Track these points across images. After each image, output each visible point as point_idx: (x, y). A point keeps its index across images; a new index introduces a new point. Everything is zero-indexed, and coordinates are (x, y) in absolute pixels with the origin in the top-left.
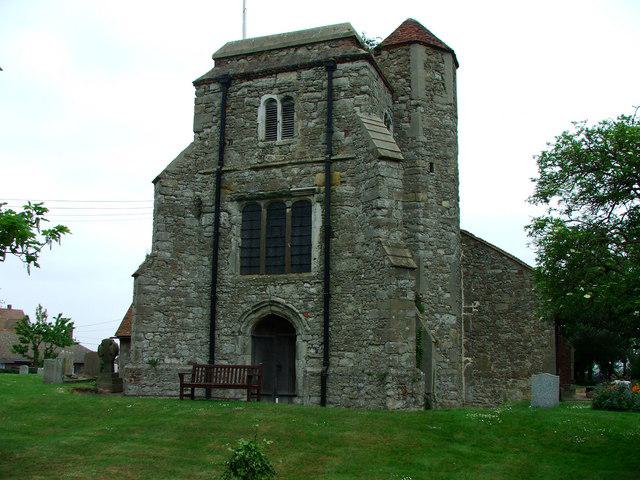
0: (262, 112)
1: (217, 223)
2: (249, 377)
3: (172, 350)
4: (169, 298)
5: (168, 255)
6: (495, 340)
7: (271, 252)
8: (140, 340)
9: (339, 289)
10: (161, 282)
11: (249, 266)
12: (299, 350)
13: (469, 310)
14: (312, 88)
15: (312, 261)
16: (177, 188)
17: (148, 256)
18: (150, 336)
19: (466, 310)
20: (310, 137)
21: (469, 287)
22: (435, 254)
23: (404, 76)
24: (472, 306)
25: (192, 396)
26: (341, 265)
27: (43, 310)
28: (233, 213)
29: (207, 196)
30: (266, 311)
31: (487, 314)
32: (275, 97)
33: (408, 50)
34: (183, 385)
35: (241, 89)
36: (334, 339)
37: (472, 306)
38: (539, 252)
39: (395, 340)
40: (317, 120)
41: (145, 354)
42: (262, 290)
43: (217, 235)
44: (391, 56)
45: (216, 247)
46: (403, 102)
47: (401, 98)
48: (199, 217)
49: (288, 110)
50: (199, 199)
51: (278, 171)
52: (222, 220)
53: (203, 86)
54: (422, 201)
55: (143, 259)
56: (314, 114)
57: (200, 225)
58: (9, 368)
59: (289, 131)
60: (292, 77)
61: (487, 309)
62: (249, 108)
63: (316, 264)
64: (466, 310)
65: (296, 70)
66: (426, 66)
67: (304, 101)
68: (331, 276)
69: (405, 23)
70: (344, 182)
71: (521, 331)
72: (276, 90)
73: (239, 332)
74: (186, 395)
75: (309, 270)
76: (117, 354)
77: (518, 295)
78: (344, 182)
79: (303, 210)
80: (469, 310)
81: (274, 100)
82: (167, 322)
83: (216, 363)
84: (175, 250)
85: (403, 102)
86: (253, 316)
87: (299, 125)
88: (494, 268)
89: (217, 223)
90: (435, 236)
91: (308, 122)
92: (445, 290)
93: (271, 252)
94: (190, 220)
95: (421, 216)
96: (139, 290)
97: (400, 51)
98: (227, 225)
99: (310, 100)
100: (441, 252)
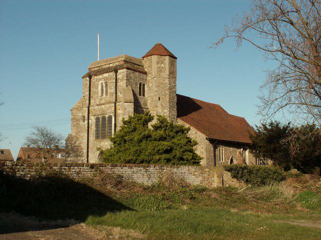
0: (100, 87)
11: (97, 137)
28: (93, 120)
35: (94, 78)
43: (88, 127)
51: (104, 106)
56: (113, 87)
59: (106, 94)
60: (106, 75)
66: (158, 63)
79: (110, 117)
87: (109, 91)
94: (81, 123)
97: (149, 58)
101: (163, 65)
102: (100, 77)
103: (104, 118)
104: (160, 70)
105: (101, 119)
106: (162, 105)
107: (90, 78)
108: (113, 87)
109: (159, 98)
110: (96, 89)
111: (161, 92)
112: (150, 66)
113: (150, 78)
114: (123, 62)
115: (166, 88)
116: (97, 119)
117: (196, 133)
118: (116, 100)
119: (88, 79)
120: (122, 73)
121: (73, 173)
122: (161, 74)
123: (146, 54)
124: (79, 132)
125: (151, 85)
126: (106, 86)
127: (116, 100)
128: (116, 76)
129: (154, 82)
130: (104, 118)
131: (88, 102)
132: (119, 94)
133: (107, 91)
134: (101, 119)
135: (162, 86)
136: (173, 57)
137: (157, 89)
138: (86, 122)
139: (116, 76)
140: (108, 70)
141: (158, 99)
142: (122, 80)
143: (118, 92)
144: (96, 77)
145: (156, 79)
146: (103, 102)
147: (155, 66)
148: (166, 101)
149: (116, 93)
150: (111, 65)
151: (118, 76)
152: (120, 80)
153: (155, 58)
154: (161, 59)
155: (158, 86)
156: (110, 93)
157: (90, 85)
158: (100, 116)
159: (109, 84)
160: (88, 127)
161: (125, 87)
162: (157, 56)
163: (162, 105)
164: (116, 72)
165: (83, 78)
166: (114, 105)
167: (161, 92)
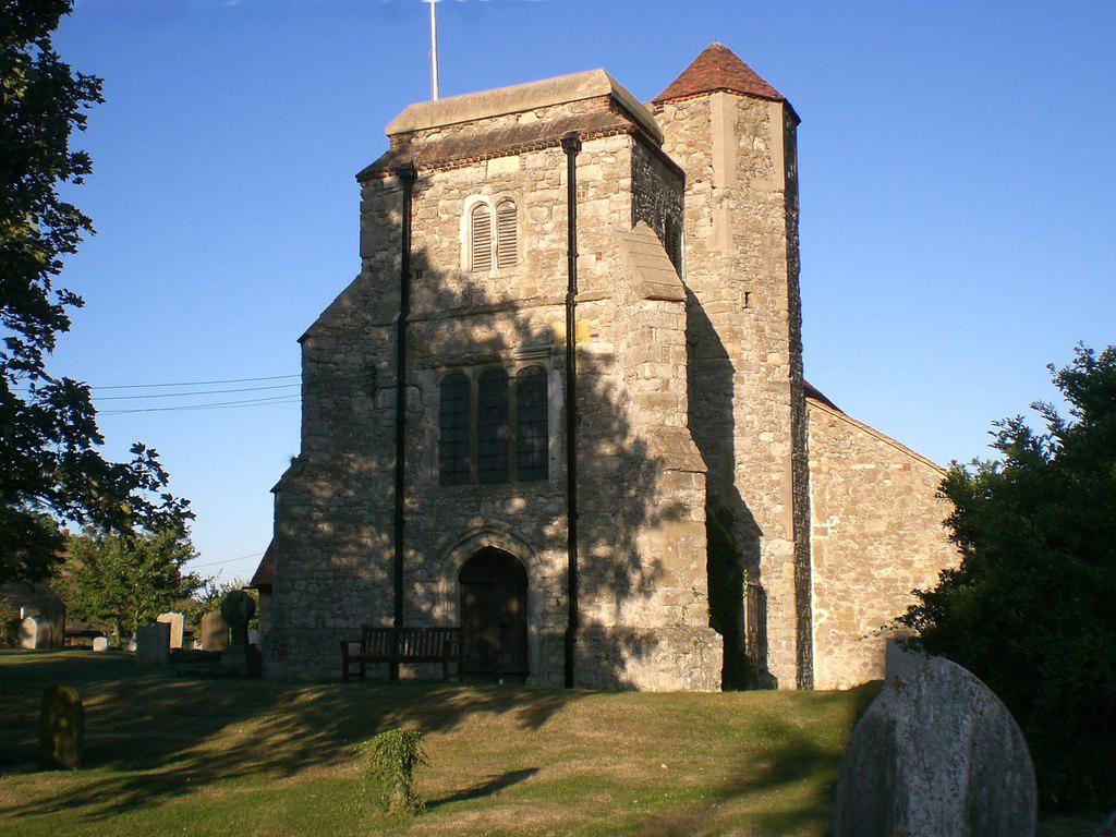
0: (465, 224)
1: (401, 405)
3: (336, 606)
5: (327, 457)
6: (866, 578)
9: (591, 505)
13: (824, 532)
14: (544, 184)
15: (550, 462)
17: (294, 460)
21: (822, 492)
24: (828, 525)
25: (362, 676)
27: (69, 310)
28: (426, 389)
31: (853, 537)
32: (485, 199)
33: (706, 103)
34: (347, 659)
37: (828, 525)
43: (401, 422)
44: (680, 115)
45: (400, 441)
46: (700, 192)
47: (696, 186)
48: (373, 395)
49: (507, 216)
50: (373, 367)
52: (409, 401)
55: (287, 466)
56: (549, 226)
57: (375, 408)
58: (41, 807)
60: (508, 165)
61: (851, 529)
62: (445, 217)
63: (557, 467)
66: (738, 129)
67: (531, 205)
68: (579, 486)
70: (596, 336)
71: (908, 564)
74: (352, 675)
75: (545, 476)
76: (251, 615)
77: (903, 504)
78: (596, 336)
81: (482, 204)
83: (405, 625)
85: (700, 192)
87: (525, 243)
89: (401, 405)
94: (360, 405)
96: (282, 514)
97: (693, 102)
98: (419, 407)
99: (540, 203)
101: (759, 144)
102: (470, 173)
104: (747, 166)
106: (760, 330)
108: (549, 226)
110: (444, 233)
112: (700, 143)
113: (701, 199)
114: (602, 106)
118: (572, 289)
121: (532, 572)
122: (754, 183)
126: (507, 216)
127: (572, 289)
128: (571, 168)
129: (721, 215)
132: (585, 258)
138: (386, 397)
139: (571, 168)
142: (606, 190)
143: (580, 250)
148: (776, 313)
149: (572, 254)
150: (527, 119)
152: (591, 192)
153: (721, 105)
156: (535, 255)
158: (468, 371)
159: (523, 210)
161: (627, 225)
162: (734, 98)
163: (760, 330)
164: (572, 146)
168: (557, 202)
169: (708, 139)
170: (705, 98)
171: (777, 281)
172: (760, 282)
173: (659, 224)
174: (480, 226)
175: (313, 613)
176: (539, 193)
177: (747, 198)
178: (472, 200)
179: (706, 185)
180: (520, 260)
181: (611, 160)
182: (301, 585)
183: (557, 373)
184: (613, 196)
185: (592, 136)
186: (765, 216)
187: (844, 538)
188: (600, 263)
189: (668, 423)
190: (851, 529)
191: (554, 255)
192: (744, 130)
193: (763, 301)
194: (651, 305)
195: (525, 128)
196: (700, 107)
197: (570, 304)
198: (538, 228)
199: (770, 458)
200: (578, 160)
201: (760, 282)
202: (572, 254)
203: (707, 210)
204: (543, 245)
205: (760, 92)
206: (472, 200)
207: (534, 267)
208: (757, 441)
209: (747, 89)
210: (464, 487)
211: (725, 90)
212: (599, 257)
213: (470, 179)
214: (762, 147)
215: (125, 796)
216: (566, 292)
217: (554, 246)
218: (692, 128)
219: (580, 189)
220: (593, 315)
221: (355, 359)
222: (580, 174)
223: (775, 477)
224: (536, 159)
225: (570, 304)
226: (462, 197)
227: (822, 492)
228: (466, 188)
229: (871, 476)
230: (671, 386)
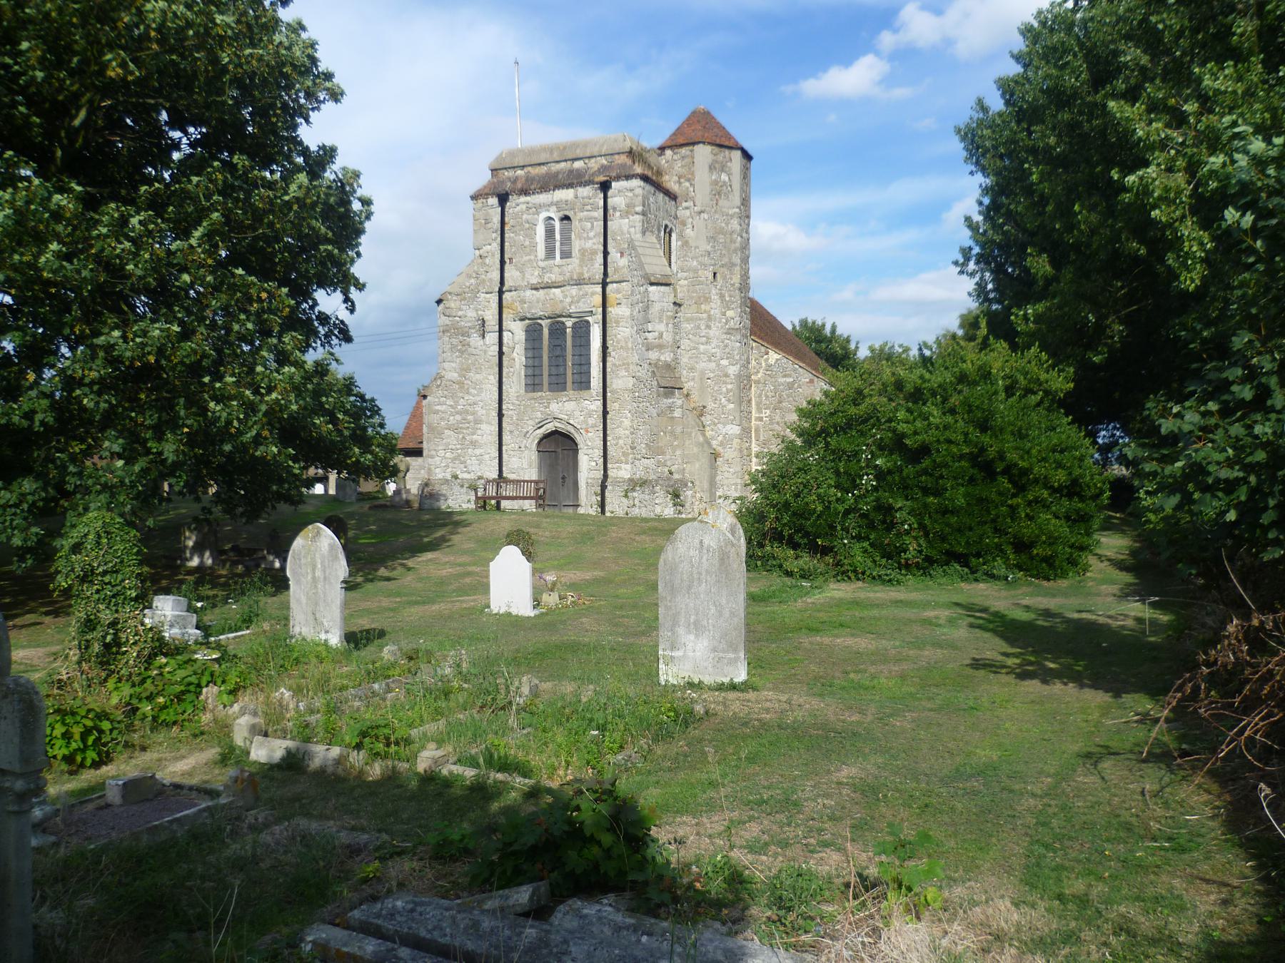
0: (541, 231)
2: (538, 490)
4: (458, 417)
5: (456, 375)
7: (554, 371)
8: (432, 457)
10: (450, 402)
11: (533, 384)
12: (580, 464)
13: (760, 419)
14: (589, 207)
16: (460, 309)
18: (441, 453)
19: (757, 419)
20: (586, 255)
21: (760, 396)
22: (718, 365)
23: (689, 180)
26: (614, 383)
28: (516, 333)
29: (491, 316)
30: (550, 427)
31: (778, 423)
32: (552, 215)
33: (692, 151)
35: (517, 204)
36: (611, 451)
38: (366, 480)
39: (663, 453)
40: (594, 240)
41: (438, 470)
42: (546, 407)
43: (501, 353)
44: (675, 157)
47: (684, 204)
51: (557, 291)
53: (480, 201)
54: (705, 311)
56: (591, 234)
59: (566, 255)
60: (565, 194)
61: (777, 418)
62: (527, 225)
64: (757, 419)
65: (572, 187)
66: (712, 168)
67: (581, 220)
69: (694, 113)
72: (554, 208)
73: (526, 447)
75: (588, 388)
79: (582, 329)
80: (760, 419)
81: (550, 218)
82: (457, 439)
84: (462, 369)
86: (538, 431)
87: (576, 245)
88: (785, 376)
90: (718, 347)
91: (586, 238)
92: (729, 401)
93: (554, 371)
94: (475, 339)
95: (703, 327)
97: (684, 151)
100: (725, 362)
101: (724, 177)
103: (557, 330)
104: (718, 192)
105: (546, 331)
106: (722, 296)
107: (503, 199)
109: (715, 274)
111: (722, 255)
113: (687, 213)
115: (733, 246)
116: (533, 333)
117: (811, 381)
118: (605, 274)
119: (494, 201)
120: (626, 192)
122: (720, 203)
123: (678, 132)
124: (468, 370)
125: (688, 231)
127: (605, 274)
128: (605, 198)
130: (557, 330)
131: (496, 275)
132: (614, 254)
133: (566, 240)
134: (546, 331)
135: (721, 238)
136: (747, 156)
137: (709, 248)
138: (492, 338)
139: (605, 198)
140: (574, 180)
141: (711, 276)
142: (627, 213)
143: (610, 249)
144: (523, 199)
145: (705, 216)
146: (549, 277)
147: (703, 177)
148: (733, 285)
149: (606, 253)
151: (609, 200)
152: (618, 214)
153: (703, 153)
154: (720, 158)
155: (712, 239)
156: (583, 251)
157: (503, 223)
160: (501, 353)
162: (708, 148)
164: (605, 187)
165: (474, 197)
166: (599, 289)
167: (722, 255)
168: (596, 219)
169: (693, 174)
170: (691, 148)
171: (734, 265)
172: (722, 266)
173: (659, 231)
174: (550, 233)
175: (449, 470)
176: (585, 213)
177: (716, 212)
178: (544, 215)
179: (690, 204)
180: (573, 255)
181: (630, 194)
182: (441, 453)
183: (596, 325)
184: (631, 217)
185: (618, 178)
186: (727, 224)
187: (772, 424)
188: (623, 259)
189: (662, 358)
190: (777, 418)
191: (594, 252)
192: (715, 168)
193: (724, 278)
194: (654, 288)
195: (577, 170)
196: (688, 153)
197: (604, 284)
198: (585, 235)
199: (727, 375)
200: (610, 193)
201: (722, 266)
202: (606, 253)
203: (690, 220)
204: (589, 244)
205: (727, 143)
206: (544, 215)
207: (582, 260)
208: (718, 365)
209: (718, 142)
210: (540, 394)
211: (704, 143)
212: (622, 254)
213: (542, 201)
214: (727, 179)
215: (201, 229)
216: (602, 276)
217: (595, 247)
218: (682, 166)
219: (610, 212)
220: (618, 291)
221: (471, 314)
222: (600, 403)
223: (730, 387)
224: (585, 191)
225: (604, 284)
226: (538, 214)
227: (760, 396)
228: (539, 208)
229: (790, 386)
230: (664, 336)
